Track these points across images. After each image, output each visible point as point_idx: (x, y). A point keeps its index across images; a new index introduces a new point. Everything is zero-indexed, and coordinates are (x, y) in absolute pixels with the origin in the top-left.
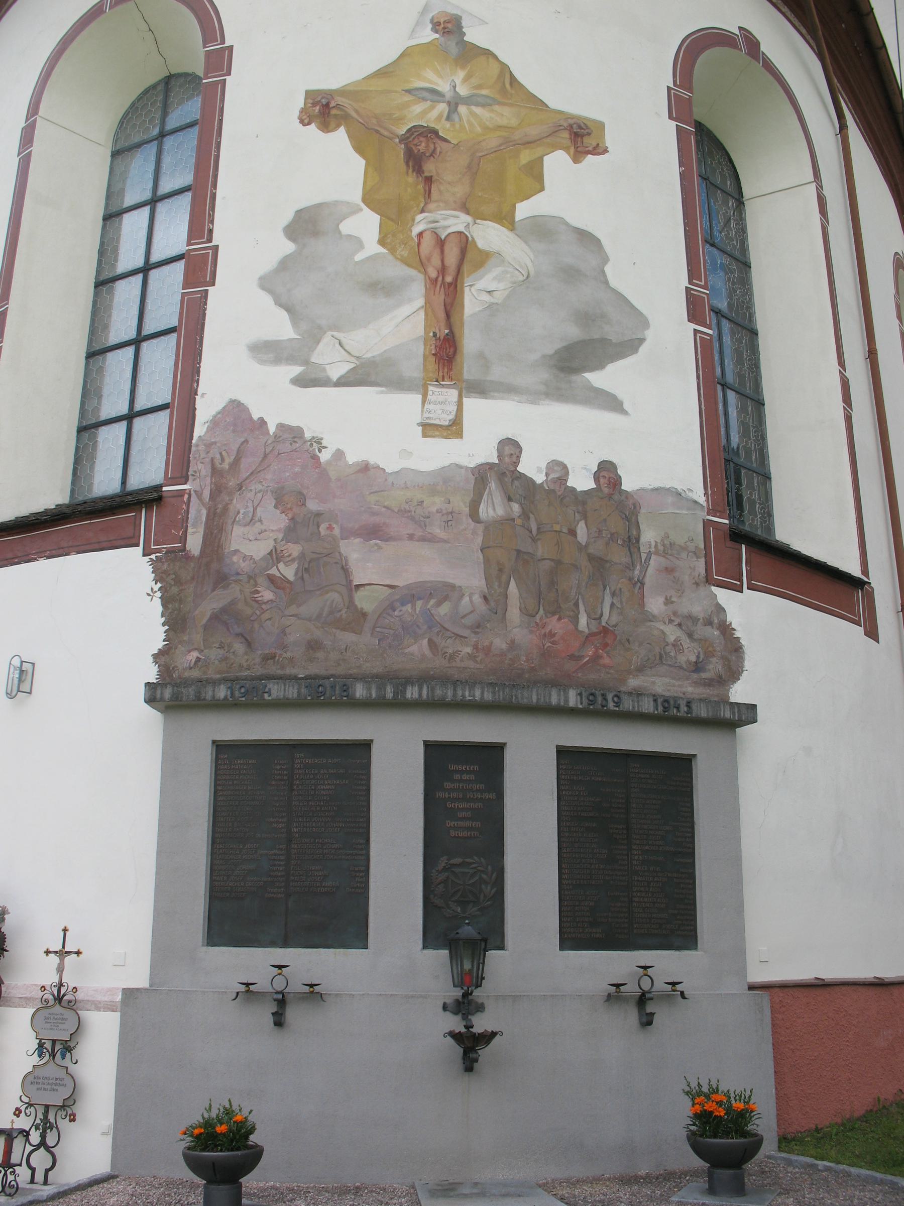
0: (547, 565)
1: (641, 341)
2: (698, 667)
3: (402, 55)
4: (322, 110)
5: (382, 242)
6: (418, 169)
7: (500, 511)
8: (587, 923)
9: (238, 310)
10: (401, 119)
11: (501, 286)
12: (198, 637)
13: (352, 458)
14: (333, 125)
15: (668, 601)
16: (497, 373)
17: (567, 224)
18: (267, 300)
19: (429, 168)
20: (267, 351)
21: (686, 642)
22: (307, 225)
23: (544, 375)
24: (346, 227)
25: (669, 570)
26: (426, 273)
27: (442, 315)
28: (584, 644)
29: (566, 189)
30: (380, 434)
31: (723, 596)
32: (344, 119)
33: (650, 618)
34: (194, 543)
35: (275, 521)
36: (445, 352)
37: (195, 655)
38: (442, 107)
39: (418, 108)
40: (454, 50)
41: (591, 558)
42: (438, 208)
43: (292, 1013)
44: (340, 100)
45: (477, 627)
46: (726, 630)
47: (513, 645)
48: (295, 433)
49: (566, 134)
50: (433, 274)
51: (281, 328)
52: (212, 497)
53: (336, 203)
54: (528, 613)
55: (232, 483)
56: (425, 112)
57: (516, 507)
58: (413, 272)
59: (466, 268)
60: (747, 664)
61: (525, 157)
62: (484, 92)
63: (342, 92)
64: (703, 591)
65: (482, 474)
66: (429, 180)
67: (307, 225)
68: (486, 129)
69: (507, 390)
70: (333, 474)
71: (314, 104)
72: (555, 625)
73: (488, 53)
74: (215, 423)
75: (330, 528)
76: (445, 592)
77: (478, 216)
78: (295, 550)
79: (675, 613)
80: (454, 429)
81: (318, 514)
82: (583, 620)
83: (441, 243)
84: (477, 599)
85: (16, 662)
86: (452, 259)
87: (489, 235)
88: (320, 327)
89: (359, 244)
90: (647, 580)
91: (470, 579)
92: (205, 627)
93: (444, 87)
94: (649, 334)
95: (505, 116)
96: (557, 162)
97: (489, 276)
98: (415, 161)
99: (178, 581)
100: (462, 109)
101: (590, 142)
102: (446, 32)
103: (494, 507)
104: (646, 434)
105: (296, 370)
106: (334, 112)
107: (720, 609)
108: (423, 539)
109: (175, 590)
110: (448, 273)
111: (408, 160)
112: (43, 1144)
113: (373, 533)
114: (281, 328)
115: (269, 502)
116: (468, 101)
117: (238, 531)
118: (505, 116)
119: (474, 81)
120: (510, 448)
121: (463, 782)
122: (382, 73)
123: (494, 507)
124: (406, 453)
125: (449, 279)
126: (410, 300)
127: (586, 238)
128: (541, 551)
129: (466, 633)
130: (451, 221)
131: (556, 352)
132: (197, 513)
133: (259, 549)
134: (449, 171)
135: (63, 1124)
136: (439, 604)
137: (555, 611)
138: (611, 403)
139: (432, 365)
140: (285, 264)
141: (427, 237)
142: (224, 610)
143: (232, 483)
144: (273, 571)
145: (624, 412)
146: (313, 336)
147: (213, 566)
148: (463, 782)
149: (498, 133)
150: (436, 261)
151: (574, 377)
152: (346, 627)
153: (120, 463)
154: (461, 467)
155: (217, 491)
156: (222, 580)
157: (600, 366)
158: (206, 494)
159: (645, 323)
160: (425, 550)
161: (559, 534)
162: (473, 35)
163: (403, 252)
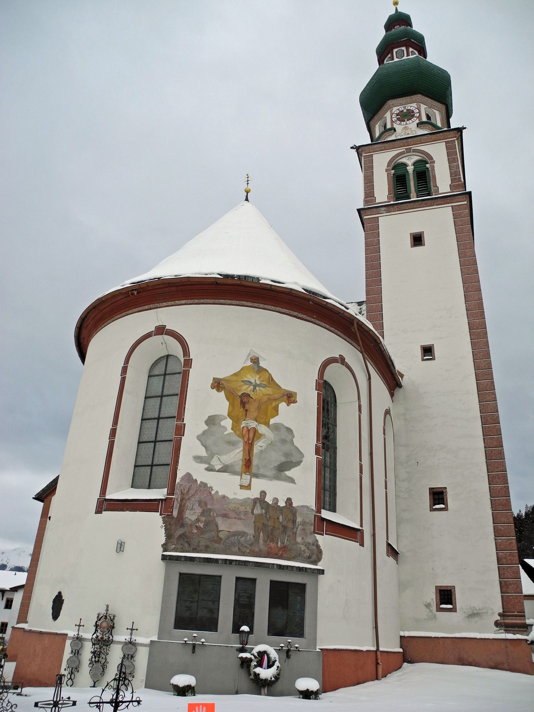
0: (271, 527)
1: (301, 461)
2: (309, 557)
3: (242, 369)
4: (218, 385)
5: (232, 429)
6: (244, 407)
7: (259, 512)
8: (275, 630)
9: (190, 446)
10: (240, 390)
11: (264, 445)
12: (175, 541)
13: (220, 494)
14: (220, 390)
15: (303, 539)
16: (261, 471)
17: (283, 425)
18: (199, 443)
19: (247, 406)
20: (198, 459)
21: (307, 550)
22: (212, 421)
23: (274, 472)
24: (223, 423)
25: (304, 530)
26: (244, 440)
27: (248, 453)
28: (279, 551)
29: (285, 415)
30: (228, 487)
31: (318, 537)
32: (224, 388)
33: (297, 543)
34: (175, 513)
35: (199, 510)
36: (248, 464)
37: (174, 546)
38: (252, 387)
39: (245, 387)
40: (256, 368)
41: (283, 526)
42: (249, 420)
43: (197, 649)
44: (223, 382)
45: (251, 545)
46: (318, 547)
47: (260, 550)
48: (205, 485)
49: (286, 397)
50: (246, 440)
51: (203, 452)
52: (181, 501)
53: (220, 415)
54: (265, 541)
55: (187, 497)
56: (247, 389)
57: (264, 511)
58: (240, 439)
59: (255, 439)
60: (323, 557)
61: (274, 404)
62: (264, 383)
63: (223, 379)
64: (312, 536)
65: (255, 501)
66: (246, 410)
67: (212, 421)
68: (264, 395)
69: (263, 476)
70: (215, 498)
71: (215, 383)
72: (272, 545)
73: (266, 370)
74: (182, 479)
75: (213, 513)
76: (243, 534)
77: (259, 423)
78: (203, 519)
79: (304, 542)
80: (248, 487)
81: (210, 509)
82: (279, 544)
83: (249, 431)
84: (252, 536)
85: (120, 542)
86: (251, 436)
87: (262, 429)
88: (214, 454)
89: (225, 429)
90: (297, 533)
91: (250, 531)
92: (177, 539)
93: (253, 381)
94: (304, 459)
95: (269, 391)
96: (283, 406)
97: (261, 442)
98: (243, 404)
99: (170, 524)
100: (257, 388)
101: (292, 399)
102: (254, 363)
103: (258, 511)
104: (300, 489)
105: (207, 466)
106: (221, 386)
107: (317, 541)
108: (238, 519)
109: (169, 527)
110: (250, 439)
111: (241, 403)
112: (71, 678)
113: (225, 516)
114: (203, 452)
115: (197, 504)
116: (259, 386)
117: (188, 512)
118: (269, 391)
119: (261, 379)
120: (263, 494)
121: (245, 589)
122: (236, 374)
123: (258, 511)
124: (235, 494)
125: (250, 442)
126: (239, 448)
127: (289, 430)
128: (270, 523)
129: (248, 546)
130: (252, 424)
131: (278, 465)
132: (176, 505)
133: (193, 518)
134: (252, 407)
135: (76, 673)
136: (241, 537)
137: (272, 541)
138: (292, 480)
139: (244, 468)
140: (204, 433)
141: (245, 428)
142: (183, 534)
143: (187, 497)
144: (197, 524)
145: (295, 483)
146: (212, 455)
147: (180, 520)
148: (245, 589)
149: (267, 396)
150: (247, 436)
151: (282, 473)
152: (216, 542)
153: (148, 480)
154: (249, 498)
155: (182, 500)
156: (182, 525)
157: (290, 470)
158: (179, 499)
159: (302, 455)
160: (239, 522)
161: (275, 523)
162: (262, 364)
163: (238, 433)
